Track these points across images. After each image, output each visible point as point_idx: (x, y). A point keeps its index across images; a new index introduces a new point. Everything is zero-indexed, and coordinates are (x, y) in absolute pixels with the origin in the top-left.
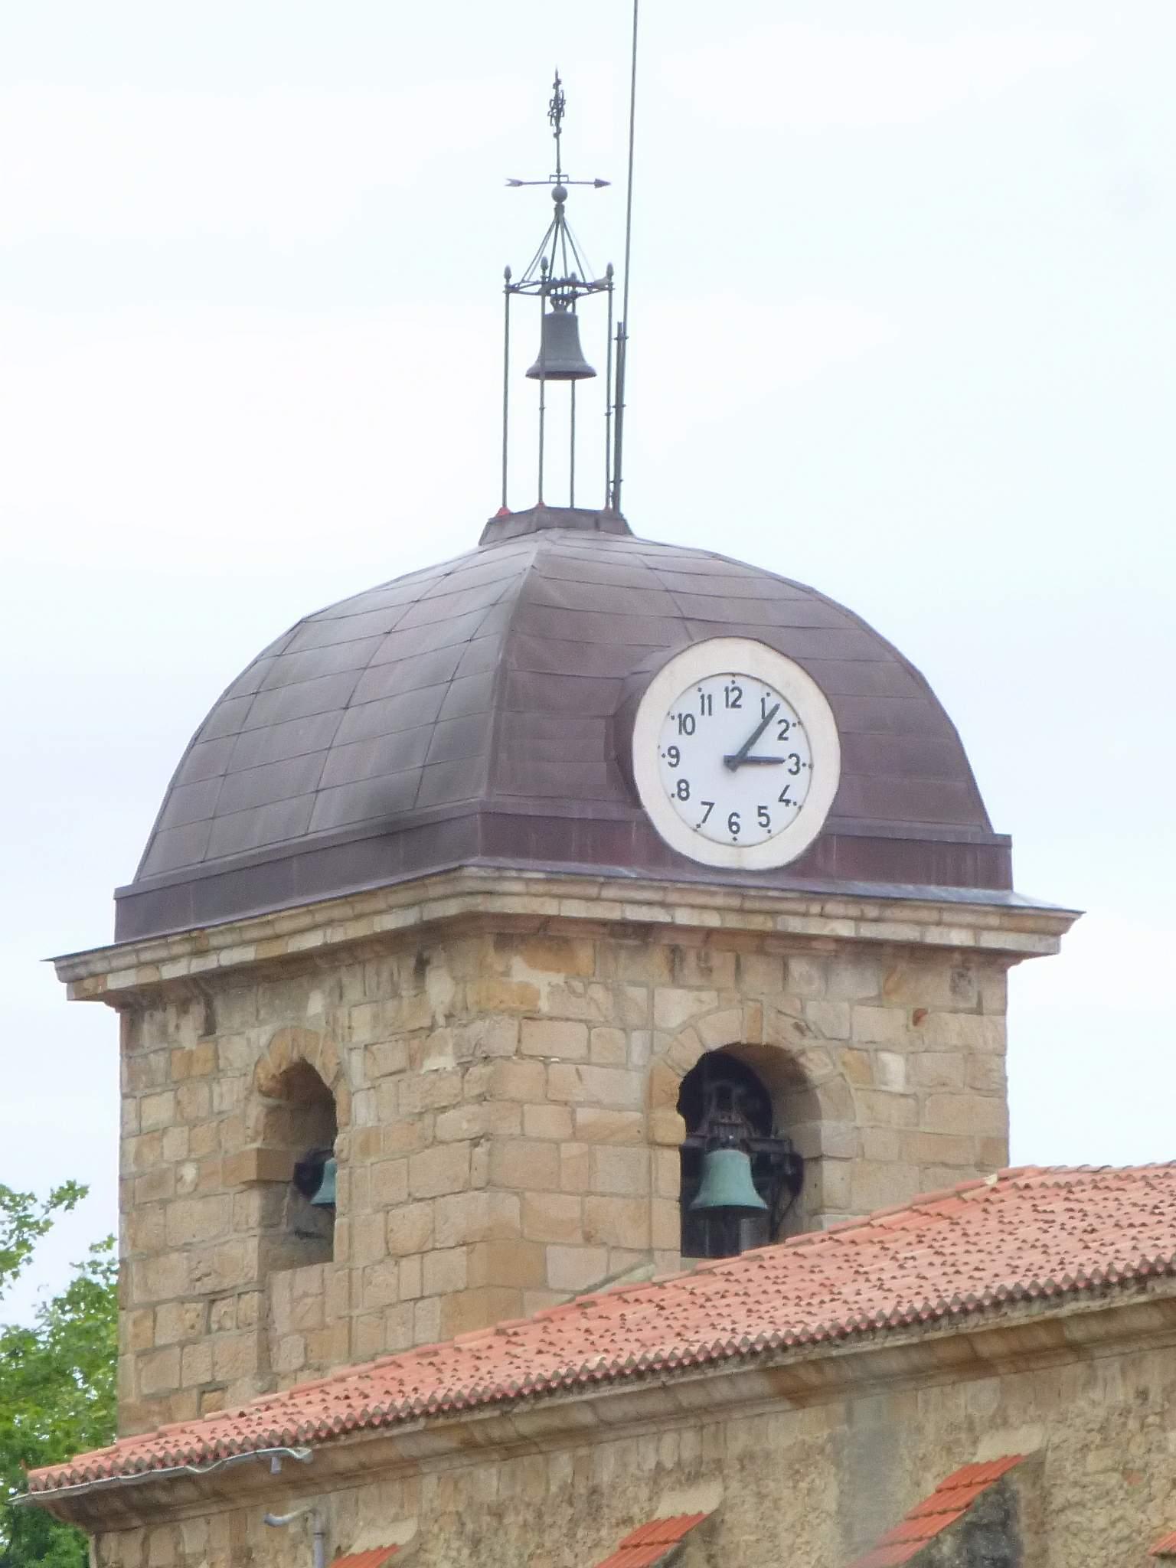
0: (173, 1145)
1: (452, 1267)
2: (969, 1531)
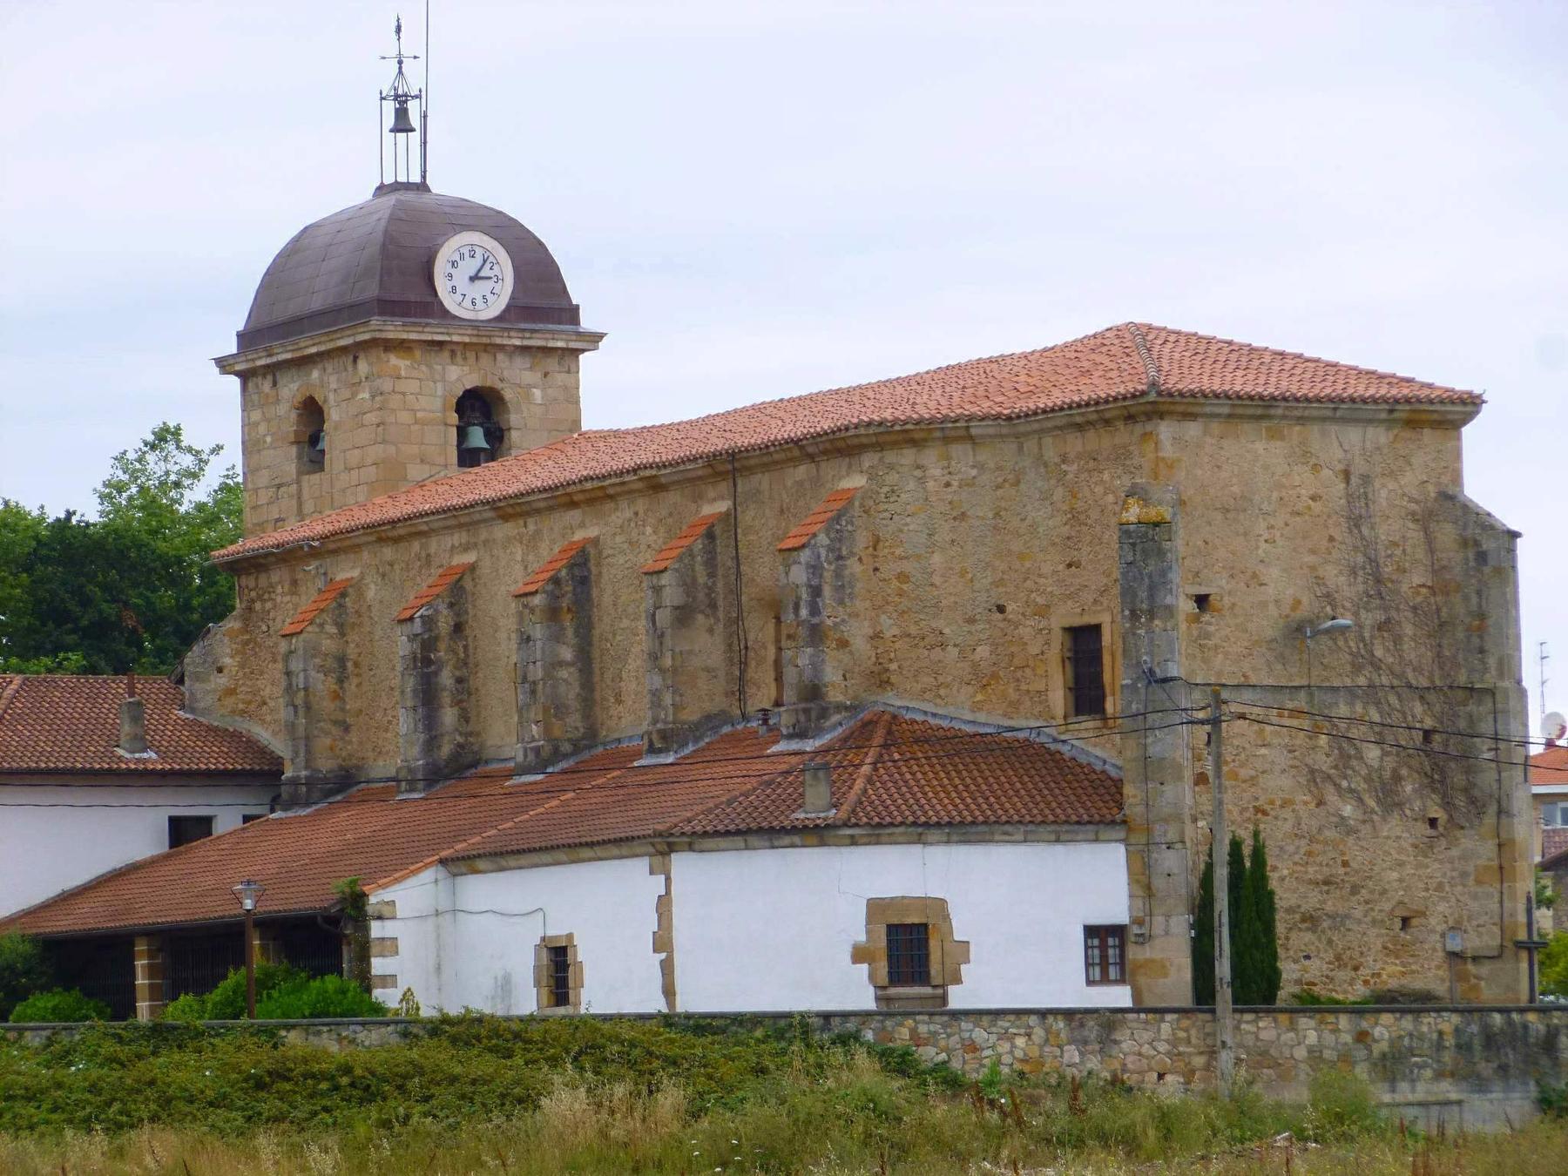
0: (262, 429)
1: (371, 473)
2: (571, 567)
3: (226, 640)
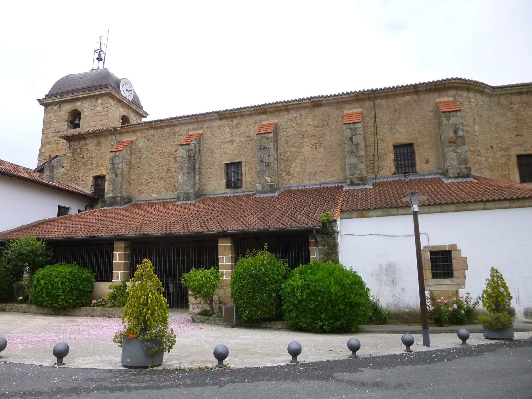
3: (66, 158)
